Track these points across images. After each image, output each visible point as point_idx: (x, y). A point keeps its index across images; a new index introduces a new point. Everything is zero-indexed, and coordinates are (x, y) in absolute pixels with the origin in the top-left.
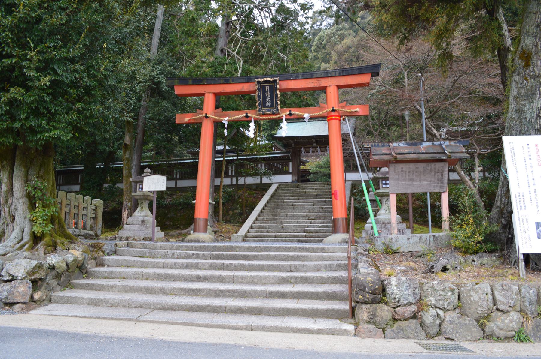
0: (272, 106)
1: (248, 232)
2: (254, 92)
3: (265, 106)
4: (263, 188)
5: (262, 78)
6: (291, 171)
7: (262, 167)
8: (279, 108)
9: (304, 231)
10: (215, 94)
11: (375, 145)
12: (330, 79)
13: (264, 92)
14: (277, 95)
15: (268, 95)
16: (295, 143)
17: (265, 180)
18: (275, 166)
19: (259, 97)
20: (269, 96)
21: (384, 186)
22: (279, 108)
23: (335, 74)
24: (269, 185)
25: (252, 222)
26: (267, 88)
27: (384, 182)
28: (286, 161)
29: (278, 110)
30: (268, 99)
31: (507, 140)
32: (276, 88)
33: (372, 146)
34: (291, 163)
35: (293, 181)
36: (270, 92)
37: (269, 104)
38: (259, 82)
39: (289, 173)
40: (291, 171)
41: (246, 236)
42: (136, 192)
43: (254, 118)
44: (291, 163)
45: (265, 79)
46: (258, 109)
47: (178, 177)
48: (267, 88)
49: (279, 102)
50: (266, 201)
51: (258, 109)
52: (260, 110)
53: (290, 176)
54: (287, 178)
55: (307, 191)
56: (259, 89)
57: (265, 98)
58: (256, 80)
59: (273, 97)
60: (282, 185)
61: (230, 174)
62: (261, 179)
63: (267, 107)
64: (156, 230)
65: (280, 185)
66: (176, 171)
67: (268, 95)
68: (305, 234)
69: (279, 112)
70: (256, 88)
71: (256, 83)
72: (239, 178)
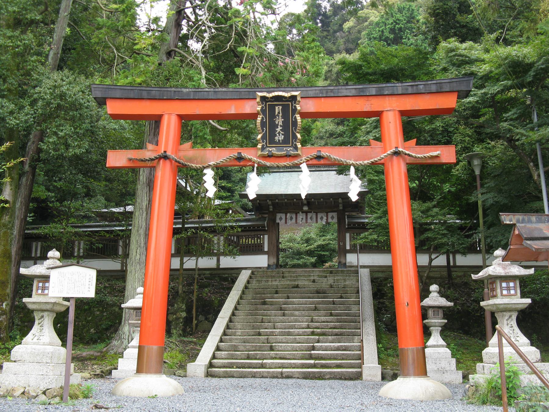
0: (286, 141)
1: (214, 357)
2: (254, 116)
3: (272, 141)
5: (269, 92)
6: (266, 249)
7: (219, 241)
8: (299, 146)
9: (311, 357)
10: (180, 117)
11: (523, 219)
12: (387, 98)
13: (273, 116)
14: (295, 123)
15: (279, 121)
16: (274, 205)
17: (227, 262)
19: (263, 124)
20: (281, 123)
21: (505, 292)
22: (299, 146)
23: (397, 89)
25: (218, 338)
26: (278, 109)
27: (504, 285)
29: (296, 148)
30: (279, 129)
32: (294, 110)
33: (518, 221)
36: (283, 117)
37: (281, 138)
38: (263, 99)
40: (266, 249)
41: (211, 365)
42: (30, 296)
43: (258, 164)
44: (266, 237)
45: (276, 94)
46: (259, 146)
48: (278, 109)
49: (299, 136)
51: (259, 146)
52: (263, 149)
53: (266, 257)
54: (261, 261)
55: (300, 283)
56: (263, 111)
57: (273, 126)
58: (260, 94)
59: (289, 126)
60: (255, 271)
62: (218, 261)
63: (275, 143)
64: (72, 370)
65: (253, 273)
66: (219, 239)
67: (279, 121)
68: (312, 362)
69: (299, 152)
70: (259, 109)
71: (258, 100)
72: (185, 259)
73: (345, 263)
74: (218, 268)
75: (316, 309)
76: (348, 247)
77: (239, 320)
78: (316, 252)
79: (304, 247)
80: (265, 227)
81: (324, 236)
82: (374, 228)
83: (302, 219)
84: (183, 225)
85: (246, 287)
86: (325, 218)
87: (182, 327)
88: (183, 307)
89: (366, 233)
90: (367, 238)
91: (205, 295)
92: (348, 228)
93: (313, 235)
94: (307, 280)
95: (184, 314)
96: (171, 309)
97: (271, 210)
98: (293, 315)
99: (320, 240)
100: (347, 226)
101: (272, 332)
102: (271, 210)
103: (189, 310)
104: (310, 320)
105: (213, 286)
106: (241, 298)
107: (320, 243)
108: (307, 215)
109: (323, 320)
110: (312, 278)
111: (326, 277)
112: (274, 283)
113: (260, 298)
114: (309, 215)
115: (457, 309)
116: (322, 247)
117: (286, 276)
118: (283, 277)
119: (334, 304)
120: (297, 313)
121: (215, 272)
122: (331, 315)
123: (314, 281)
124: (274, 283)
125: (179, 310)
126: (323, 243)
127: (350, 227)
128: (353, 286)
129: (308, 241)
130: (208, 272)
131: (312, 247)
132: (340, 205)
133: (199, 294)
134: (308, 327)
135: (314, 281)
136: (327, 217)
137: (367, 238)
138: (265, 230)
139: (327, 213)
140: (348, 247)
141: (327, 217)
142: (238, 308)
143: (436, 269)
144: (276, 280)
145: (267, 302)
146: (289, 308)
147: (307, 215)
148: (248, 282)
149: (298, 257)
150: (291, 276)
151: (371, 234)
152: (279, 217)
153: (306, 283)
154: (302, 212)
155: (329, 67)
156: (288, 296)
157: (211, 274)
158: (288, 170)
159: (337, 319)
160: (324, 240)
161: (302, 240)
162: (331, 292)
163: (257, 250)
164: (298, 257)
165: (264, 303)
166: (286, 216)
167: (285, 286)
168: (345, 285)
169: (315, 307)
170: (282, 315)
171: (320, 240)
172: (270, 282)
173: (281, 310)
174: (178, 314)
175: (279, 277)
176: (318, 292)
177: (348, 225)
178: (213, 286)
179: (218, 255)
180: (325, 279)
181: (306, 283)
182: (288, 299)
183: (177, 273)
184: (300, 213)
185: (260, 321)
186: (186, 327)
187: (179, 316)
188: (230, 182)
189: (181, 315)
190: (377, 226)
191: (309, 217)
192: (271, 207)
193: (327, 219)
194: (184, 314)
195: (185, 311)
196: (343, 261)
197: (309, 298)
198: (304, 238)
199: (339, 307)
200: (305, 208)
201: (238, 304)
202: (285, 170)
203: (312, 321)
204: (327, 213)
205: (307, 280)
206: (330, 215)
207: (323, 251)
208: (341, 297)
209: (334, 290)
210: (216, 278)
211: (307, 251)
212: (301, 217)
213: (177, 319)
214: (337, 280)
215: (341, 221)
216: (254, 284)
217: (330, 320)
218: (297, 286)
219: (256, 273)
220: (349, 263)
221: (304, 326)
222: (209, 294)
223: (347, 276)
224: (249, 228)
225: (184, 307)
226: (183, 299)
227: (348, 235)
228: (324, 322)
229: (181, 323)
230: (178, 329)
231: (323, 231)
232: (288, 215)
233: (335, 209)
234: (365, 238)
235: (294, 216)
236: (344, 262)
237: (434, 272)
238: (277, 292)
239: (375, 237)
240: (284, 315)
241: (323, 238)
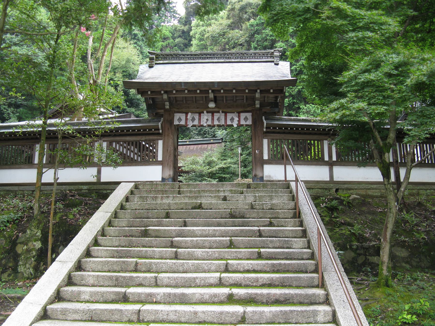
4: (99, 192)
6: (160, 158)
17: (109, 174)
18: (132, 144)
24: (114, 185)
28: (151, 137)
31: (102, 181)
34: (160, 143)
35: (163, 179)
39: (157, 163)
40: (160, 158)
44: (160, 143)
47: (334, 159)
50: (99, 227)
53: (160, 168)
54: (153, 173)
55: (204, 201)
61: (326, 158)
62: (99, 172)
65: (137, 186)
66: (101, 145)
68: (225, 291)
73: (262, 177)
74: (99, 183)
75: (231, 245)
76: (266, 157)
77: (93, 266)
78: (217, 175)
79: (206, 170)
80: (159, 130)
81: (225, 160)
82: (355, 91)
83: (207, 120)
84: (45, 123)
85: (122, 207)
86: (236, 119)
87: (34, 263)
88: (38, 234)
89: (343, 101)
90: (348, 108)
91: (71, 217)
92: (266, 132)
93: (215, 159)
94: (215, 197)
95: (38, 245)
96: (22, 237)
97: (167, 107)
98: (191, 257)
99: (221, 163)
100: (265, 130)
101: (150, 295)
102: (167, 107)
103: (44, 240)
104: (223, 268)
105: (86, 204)
106: (110, 223)
107: (221, 166)
108: (213, 116)
109: (246, 268)
110: (222, 194)
111: (242, 193)
112: (166, 201)
113: (141, 223)
114: (216, 116)
115: (423, 238)
116: (223, 170)
117: (183, 191)
118: (179, 193)
119: (260, 236)
120: (199, 252)
121: (95, 187)
122: (260, 256)
123: (225, 199)
124: (166, 201)
125: (33, 237)
126: (224, 166)
127: (268, 130)
128: (286, 207)
129: (210, 164)
130: (85, 187)
131: (214, 169)
132: (257, 102)
133: (63, 216)
134: (220, 284)
135: (225, 199)
136: (239, 117)
137: (348, 108)
138: (159, 134)
139: (239, 113)
140: (266, 157)
141: (239, 117)
142: (99, 241)
143: (375, 186)
144: (168, 197)
145: (150, 232)
146: (186, 242)
147: (213, 116)
148: (127, 199)
149: (200, 179)
150: (191, 192)
151: (353, 102)
152: (178, 118)
153: (214, 201)
154: (208, 112)
155: (232, 5)
156: (185, 222)
157: (89, 190)
158: (190, 61)
159: (273, 265)
160: (225, 164)
161: (204, 162)
162: (253, 215)
163: (147, 158)
164: (200, 179)
165: (145, 234)
166: (186, 116)
167: (180, 207)
168: (272, 204)
169: (231, 241)
170: (173, 256)
171: (221, 163)
172: (171, 199)
173: (172, 246)
174: (30, 244)
175: (173, 192)
176: (232, 216)
177: (266, 128)
178: (86, 204)
179: (99, 166)
180: (242, 196)
181: (214, 201)
182: (185, 225)
183: (48, 188)
184: (205, 112)
185: (132, 267)
186: (39, 263)
187: (32, 247)
188: (138, 110)
189: (34, 246)
190: (367, 84)
191: (216, 117)
192: (167, 103)
193: (239, 121)
194: (38, 245)
195: (40, 240)
196: (259, 174)
197: (219, 225)
198: (207, 161)
199: (271, 242)
200: (212, 105)
201: (103, 235)
202: (187, 61)
203: (227, 270)
204: (239, 113)
205: (215, 197)
206: (243, 115)
207: (224, 174)
208: (271, 224)
209: (258, 213)
210: (93, 195)
211: (209, 173)
212: (206, 117)
213: (28, 251)
214: (260, 197)
215: (257, 122)
216: (136, 202)
217: (259, 268)
218: (200, 207)
219: (140, 187)
220: (267, 176)
221: (212, 281)
222: (78, 216)
223: (272, 192)
224: (139, 130)
225: (39, 234)
226: (40, 223)
227: (265, 141)
228: (248, 271)
229: (34, 257)
230: (28, 266)
231: (224, 156)
232: (190, 114)
233: (248, 109)
234: (342, 107)
235: (196, 116)
236: (260, 175)
237: (373, 189)
238: (168, 216)
239: (362, 105)
240: (176, 257)
241: (225, 161)
